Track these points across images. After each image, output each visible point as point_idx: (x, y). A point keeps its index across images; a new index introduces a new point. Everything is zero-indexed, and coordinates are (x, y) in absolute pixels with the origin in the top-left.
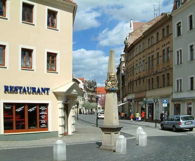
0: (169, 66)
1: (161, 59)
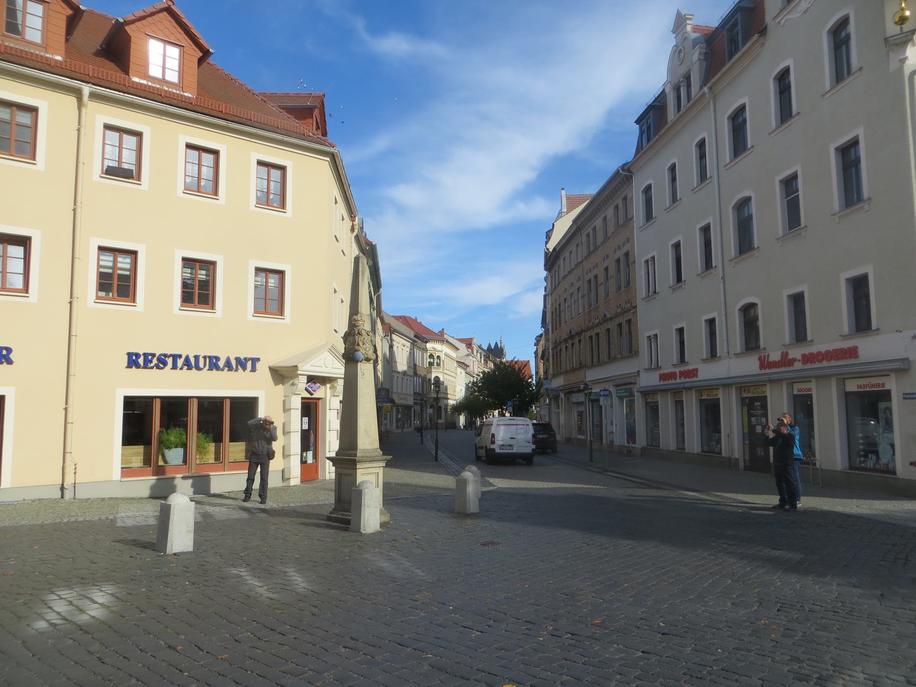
1: (612, 282)
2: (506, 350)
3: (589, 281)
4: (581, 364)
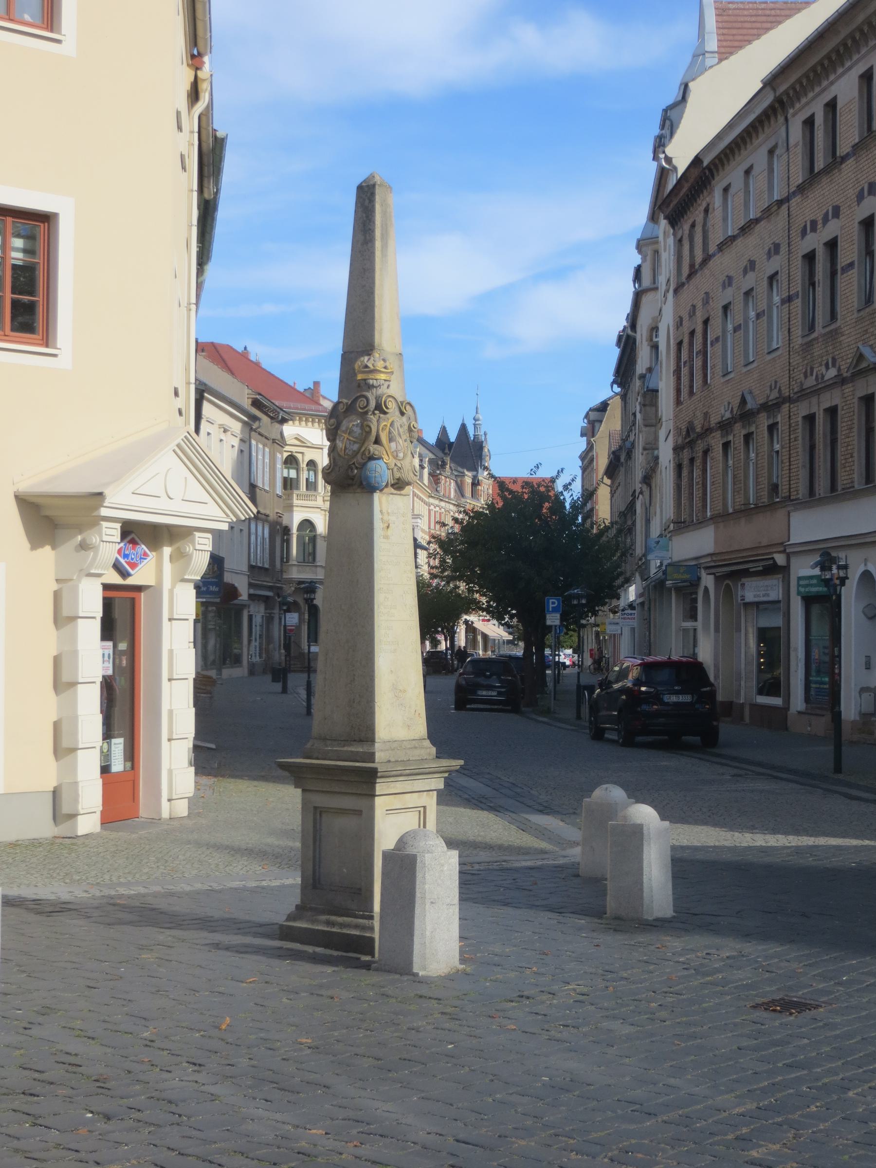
0: (834, 360)
2: (491, 446)
3: (810, 258)
4: (774, 488)
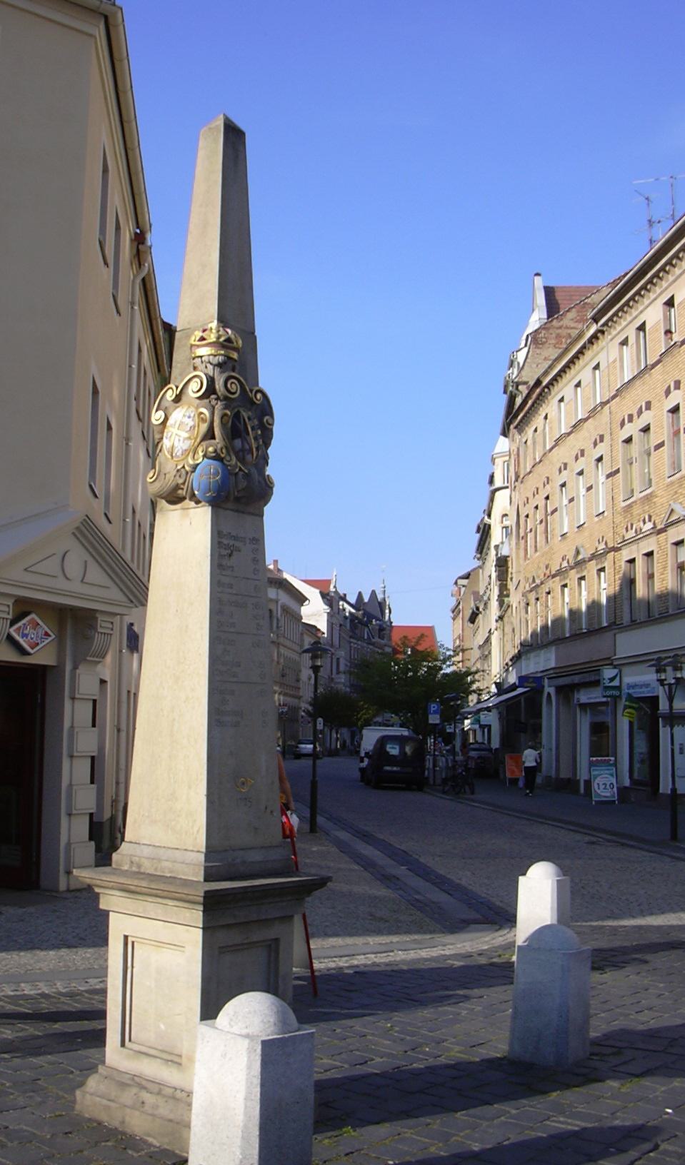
0: (650, 517)
